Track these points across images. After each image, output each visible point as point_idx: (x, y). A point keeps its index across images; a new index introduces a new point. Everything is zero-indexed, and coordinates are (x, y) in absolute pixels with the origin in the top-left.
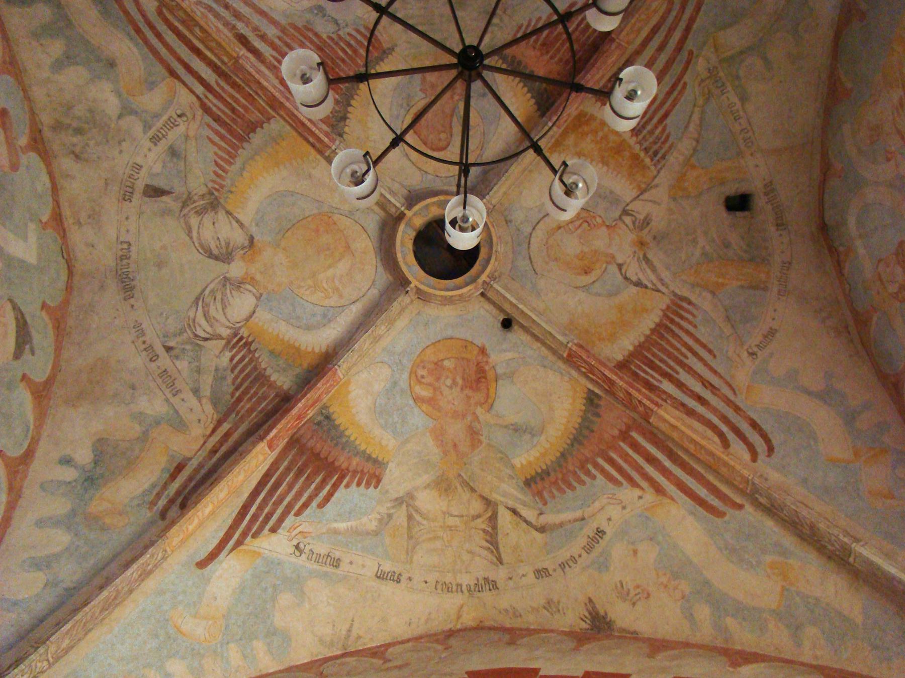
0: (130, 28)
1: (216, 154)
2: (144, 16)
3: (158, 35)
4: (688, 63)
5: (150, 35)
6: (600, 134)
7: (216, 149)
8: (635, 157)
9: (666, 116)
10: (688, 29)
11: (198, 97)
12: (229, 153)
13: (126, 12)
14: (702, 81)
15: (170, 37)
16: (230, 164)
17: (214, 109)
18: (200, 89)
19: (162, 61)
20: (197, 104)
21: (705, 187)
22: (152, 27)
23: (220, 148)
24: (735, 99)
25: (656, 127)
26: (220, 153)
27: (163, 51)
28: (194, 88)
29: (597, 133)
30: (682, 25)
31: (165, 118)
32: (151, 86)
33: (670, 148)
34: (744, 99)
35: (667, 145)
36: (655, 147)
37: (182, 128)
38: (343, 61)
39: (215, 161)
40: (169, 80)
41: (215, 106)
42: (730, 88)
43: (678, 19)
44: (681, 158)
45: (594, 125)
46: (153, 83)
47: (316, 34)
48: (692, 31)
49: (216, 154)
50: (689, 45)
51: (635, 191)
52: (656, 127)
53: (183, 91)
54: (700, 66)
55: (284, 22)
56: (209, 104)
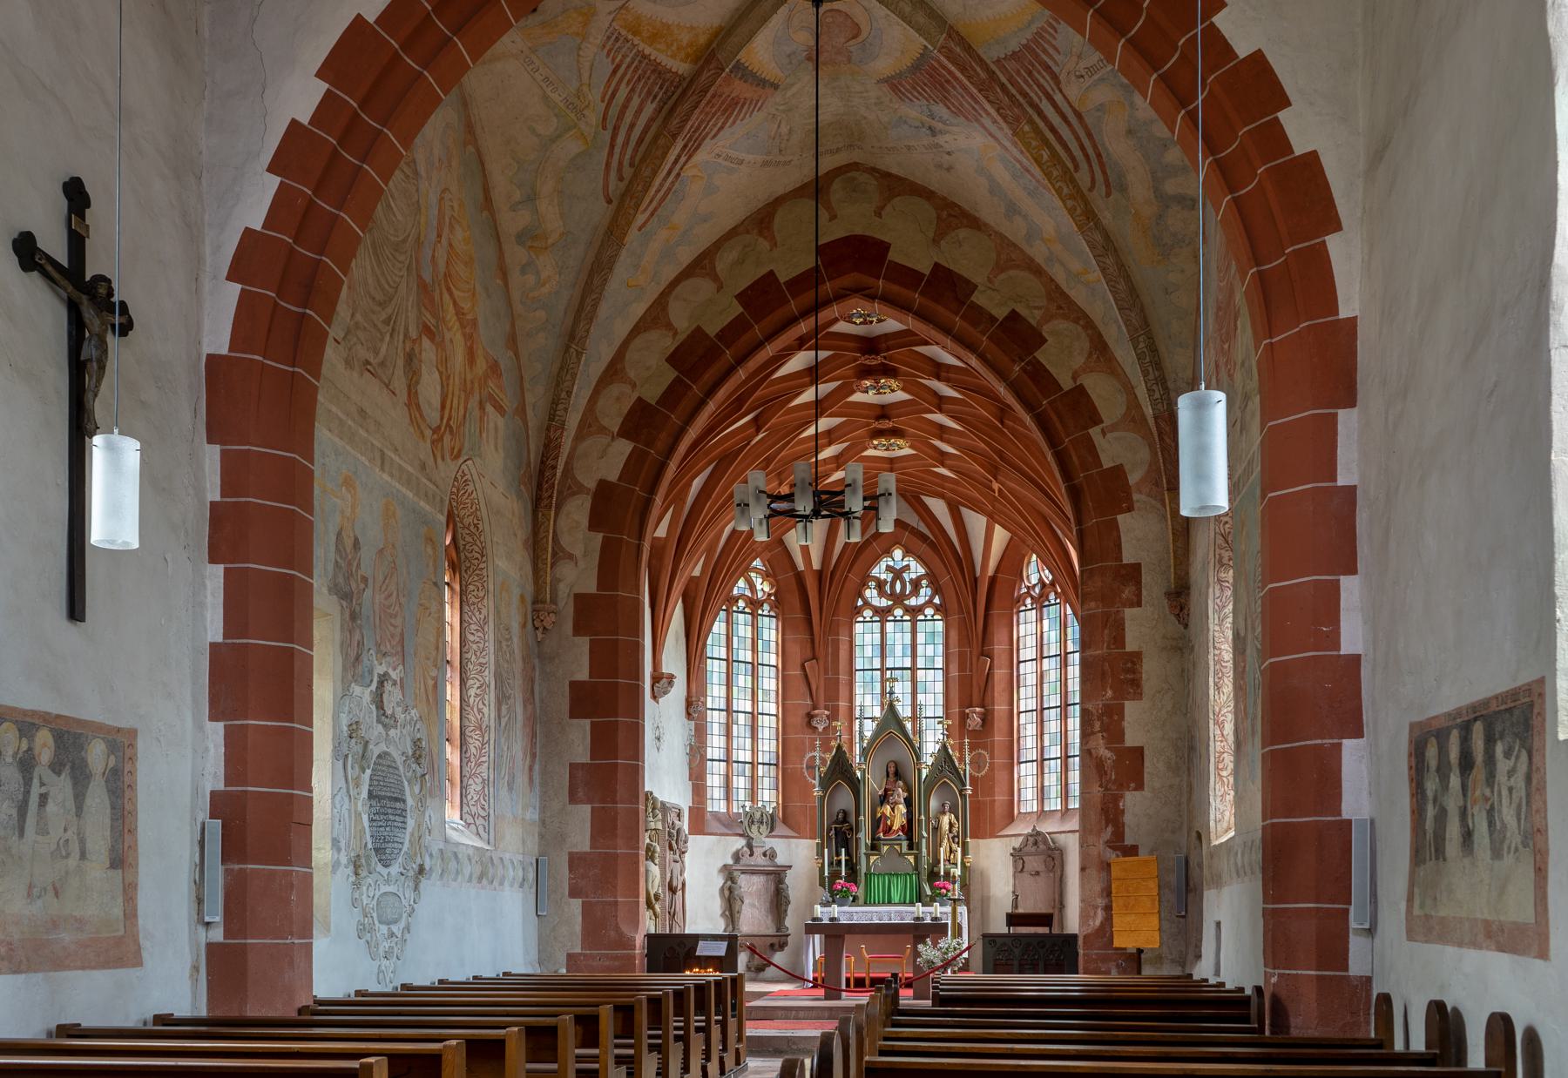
0: (1105, 159)
1: (1055, 38)
2: (1090, 166)
3: (1082, 148)
4: (604, 119)
5: (1090, 151)
6: (674, 48)
7: (1054, 42)
8: (635, 34)
9: (615, 72)
10: (612, 146)
11: (1061, 91)
12: (1042, 37)
13: (1104, 173)
14: (587, 107)
15: (1074, 146)
16: (1042, 28)
17: (1048, 78)
18: (1058, 98)
19: (1086, 128)
20: (1063, 86)
21: (560, 18)
22: (1087, 156)
23: (1049, 42)
24: (554, 96)
25: (621, 61)
26: (1051, 39)
27: (1082, 134)
28: (1062, 99)
29: (678, 49)
30: (617, 150)
31: (1096, 77)
32: (1101, 108)
33: (604, 46)
34: (545, 98)
35: (608, 47)
36: (618, 45)
37: (1082, 65)
38: (925, 85)
39: (1056, 32)
40: (1082, 110)
41: (1047, 81)
42: (561, 105)
43: (623, 153)
44: (591, 39)
45: (683, 55)
46: (1098, 110)
47: (949, 108)
48: (608, 145)
49: (1055, 38)
50: (607, 135)
51: (631, 6)
52: (621, 61)
53: (1072, 98)
54: (593, 118)
55: (976, 125)
56: (1052, 83)
